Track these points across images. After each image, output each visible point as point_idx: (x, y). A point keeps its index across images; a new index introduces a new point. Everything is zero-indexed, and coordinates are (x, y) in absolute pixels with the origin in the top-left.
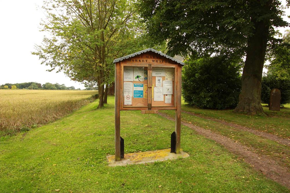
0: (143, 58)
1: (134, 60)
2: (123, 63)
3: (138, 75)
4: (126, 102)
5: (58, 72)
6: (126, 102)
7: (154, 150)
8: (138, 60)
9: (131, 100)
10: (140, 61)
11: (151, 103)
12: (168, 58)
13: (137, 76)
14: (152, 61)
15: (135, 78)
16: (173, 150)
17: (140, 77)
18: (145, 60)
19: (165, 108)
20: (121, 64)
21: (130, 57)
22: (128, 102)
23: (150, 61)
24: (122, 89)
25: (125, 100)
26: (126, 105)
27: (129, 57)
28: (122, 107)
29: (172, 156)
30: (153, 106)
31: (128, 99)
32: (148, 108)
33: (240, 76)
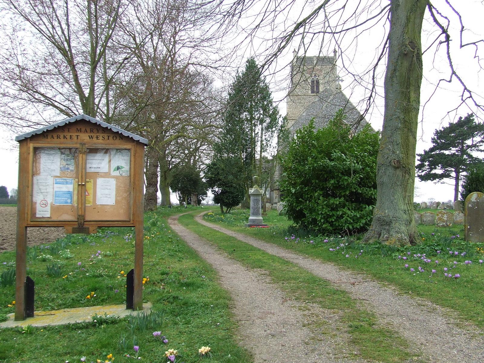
0: (71, 132)
1: (55, 135)
2: (34, 142)
3: (119, 165)
4: (41, 213)
5: (99, 168)
6: (41, 213)
7: (292, 76)
8: (62, 136)
9: (48, 208)
10: (64, 137)
11: (83, 214)
12: (106, 127)
13: (116, 166)
14: (89, 138)
15: (114, 170)
16: (130, 306)
17: (124, 167)
18: (74, 135)
19: (111, 223)
20: (28, 144)
21: (45, 131)
22: (43, 213)
23: (85, 137)
24: (30, 189)
25: (38, 207)
26: (40, 218)
27: (44, 131)
28: (29, 219)
29: (128, 313)
30: (87, 218)
31: (44, 206)
32: (77, 223)
33: (75, 207)
